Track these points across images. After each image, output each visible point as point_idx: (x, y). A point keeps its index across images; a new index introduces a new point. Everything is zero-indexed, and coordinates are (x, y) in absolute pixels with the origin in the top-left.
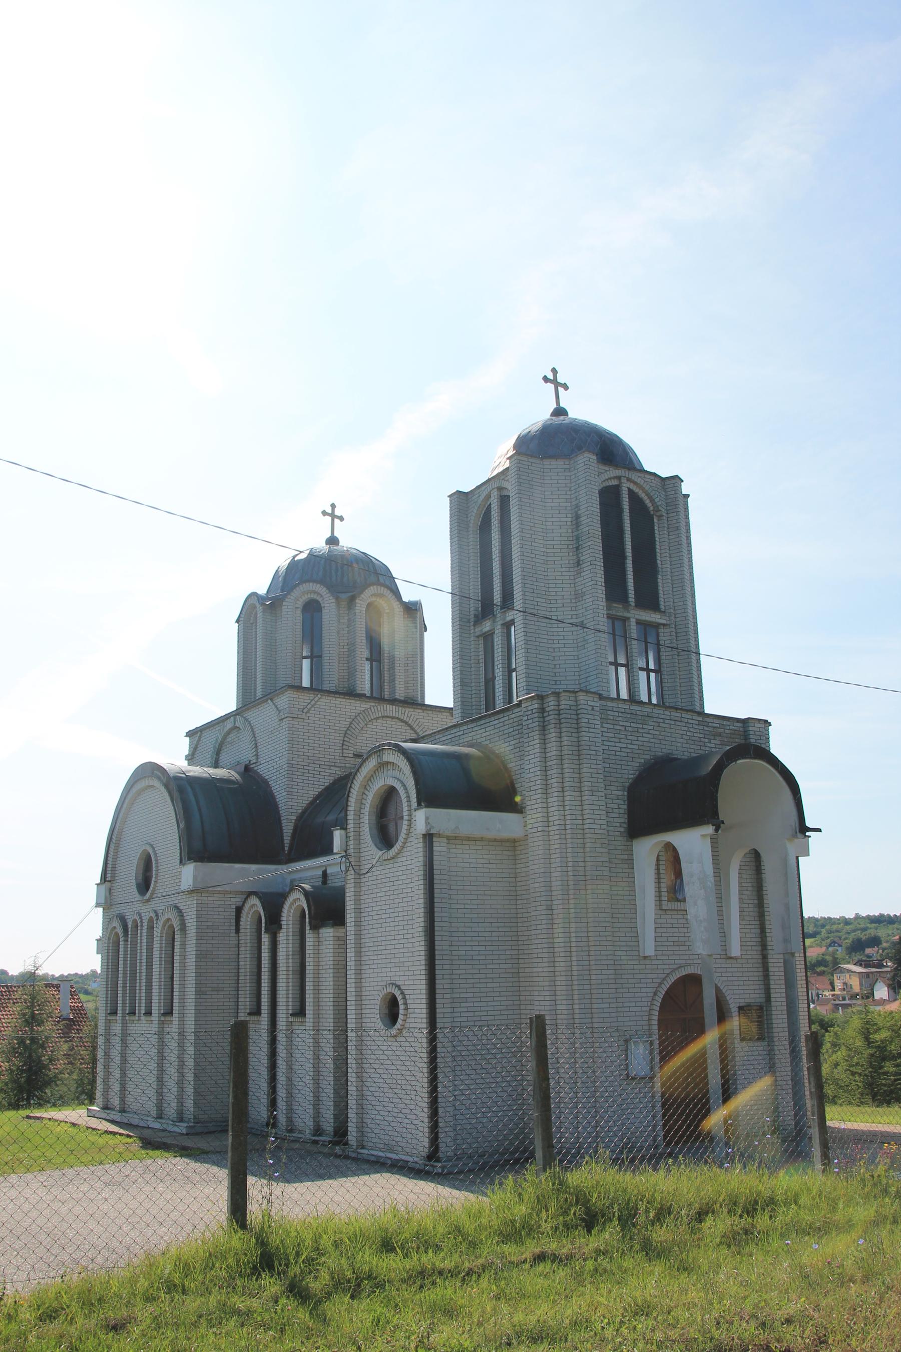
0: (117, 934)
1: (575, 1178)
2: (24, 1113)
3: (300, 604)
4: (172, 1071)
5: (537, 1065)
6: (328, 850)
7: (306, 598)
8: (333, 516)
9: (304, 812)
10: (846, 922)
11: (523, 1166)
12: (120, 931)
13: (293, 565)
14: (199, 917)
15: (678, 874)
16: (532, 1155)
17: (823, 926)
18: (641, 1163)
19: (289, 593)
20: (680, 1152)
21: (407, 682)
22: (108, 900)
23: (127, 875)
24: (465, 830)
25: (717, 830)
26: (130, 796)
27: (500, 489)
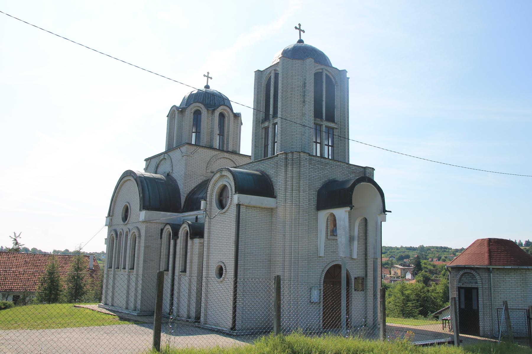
0: (113, 237)
1: (289, 338)
2: (71, 305)
3: (193, 111)
4: (132, 294)
5: (277, 295)
6: (198, 208)
7: (195, 109)
8: (208, 77)
9: (190, 193)
10: (397, 249)
11: (269, 332)
12: (114, 236)
13: (191, 96)
14: (146, 232)
15: (335, 225)
16: (272, 329)
17: (388, 250)
18: (314, 334)
19: (189, 106)
20: (329, 331)
21: (233, 145)
22: (110, 224)
23: (119, 214)
24: (253, 203)
25: (351, 209)
26: (121, 183)
27: (275, 70)
